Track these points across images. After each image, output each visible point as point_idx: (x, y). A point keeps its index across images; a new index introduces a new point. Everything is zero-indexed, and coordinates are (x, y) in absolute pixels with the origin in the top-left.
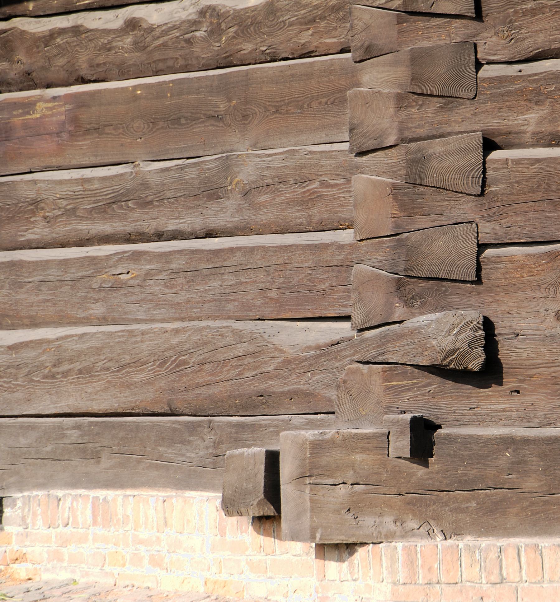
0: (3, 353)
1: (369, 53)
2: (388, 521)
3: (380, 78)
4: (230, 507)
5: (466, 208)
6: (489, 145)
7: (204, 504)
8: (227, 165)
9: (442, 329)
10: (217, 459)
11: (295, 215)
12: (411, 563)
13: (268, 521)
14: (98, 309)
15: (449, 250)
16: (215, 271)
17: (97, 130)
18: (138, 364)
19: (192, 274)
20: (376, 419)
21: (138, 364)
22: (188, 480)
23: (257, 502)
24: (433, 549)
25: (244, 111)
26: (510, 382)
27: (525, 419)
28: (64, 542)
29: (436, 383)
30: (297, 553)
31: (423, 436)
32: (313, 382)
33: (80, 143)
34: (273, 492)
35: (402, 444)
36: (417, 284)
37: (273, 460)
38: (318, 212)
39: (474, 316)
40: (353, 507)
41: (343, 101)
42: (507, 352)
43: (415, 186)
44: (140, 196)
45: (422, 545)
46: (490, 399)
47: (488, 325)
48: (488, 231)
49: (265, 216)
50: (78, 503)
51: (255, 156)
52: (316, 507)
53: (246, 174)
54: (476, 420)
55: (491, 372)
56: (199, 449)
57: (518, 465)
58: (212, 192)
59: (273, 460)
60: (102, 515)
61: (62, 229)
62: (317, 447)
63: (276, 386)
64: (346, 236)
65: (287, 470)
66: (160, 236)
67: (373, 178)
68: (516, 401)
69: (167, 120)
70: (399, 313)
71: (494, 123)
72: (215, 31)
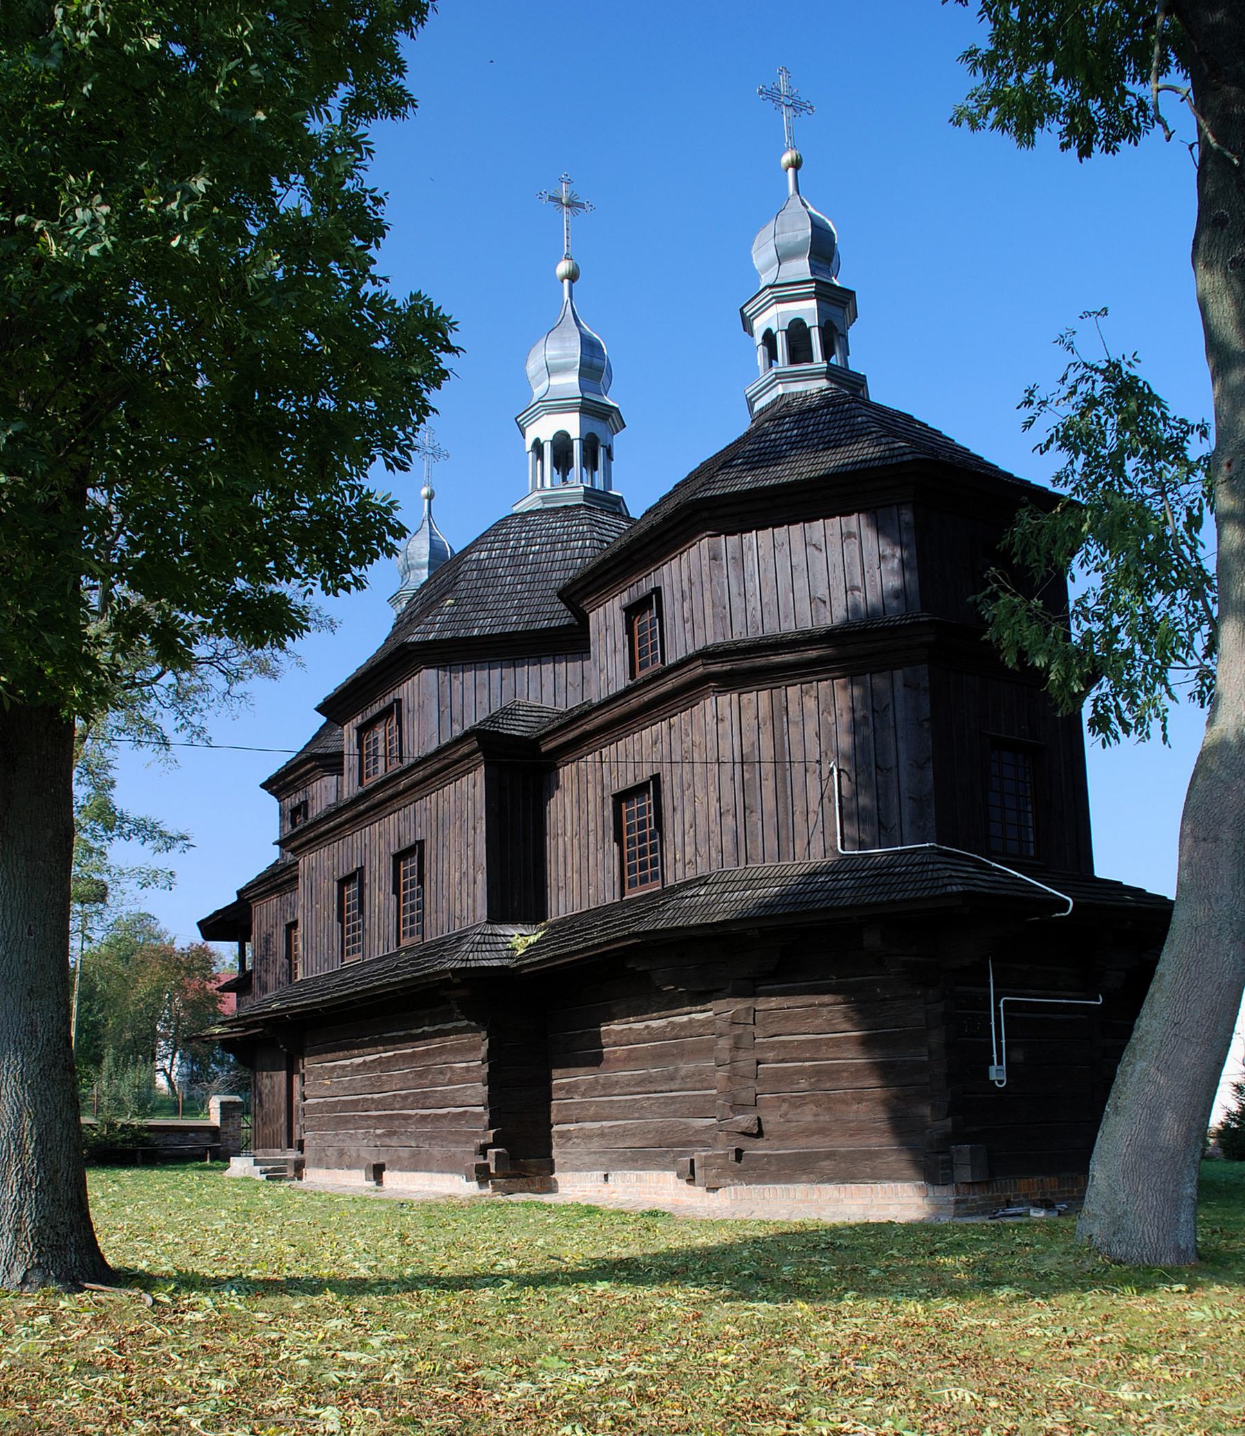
0: (1237, 1257)
1: (721, 1035)
2: (729, 1181)
3: (724, 1043)
4: (679, 1176)
5: (751, 1083)
6: (758, 1063)
7: (671, 1176)
8: (677, 1070)
9: (745, 1120)
10: (674, 1162)
11: (698, 1085)
12: (736, 1193)
13: (691, 1181)
14: (637, 1115)
15: (746, 1096)
16: (673, 1103)
17: (636, 1059)
18: (649, 1132)
19: (666, 1104)
20: (723, 1149)
21: (649, 1132)
22: (666, 1168)
23: (688, 1175)
24: (743, 1189)
25: (682, 1053)
26: (766, 1137)
27: (771, 1149)
28: (628, 1187)
29: (743, 1137)
30: (700, 1190)
31: (739, 1154)
32: (703, 1137)
33: (994, 864)
34: (692, 1172)
35: (732, 1156)
36: (738, 1107)
37: (692, 1161)
38: (705, 1084)
39: (755, 1116)
40: (718, 1176)
41: (712, 1050)
42: (765, 1128)
43: (733, 1076)
44: (649, 1080)
45: (739, 1187)
46: (760, 1142)
47: (759, 1119)
48: (758, 1090)
49: (689, 1086)
50: (632, 1175)
51: (686, 1067)
52: (706, 1176)
53: (683, 1073)
54: (757, 1149)
55: (760, 1134)
56: (669, 1159)
57: (768, 1162)
58: (672, 1078)
59: (692, 1161)
60: (639, 1179)
61: (626, 1090)
62: (706, 1157)
63: (693, 1139)
64: (714, 1092)
65: (696, 1165)
66: (656, 1092)
67: (722, 1074)
68: (768, 1143)
69: (658, 1056)
70: (731, 1115)
71: (759, 1056)
72: (673, 1029)
